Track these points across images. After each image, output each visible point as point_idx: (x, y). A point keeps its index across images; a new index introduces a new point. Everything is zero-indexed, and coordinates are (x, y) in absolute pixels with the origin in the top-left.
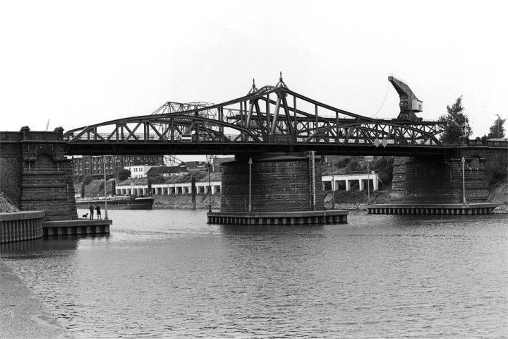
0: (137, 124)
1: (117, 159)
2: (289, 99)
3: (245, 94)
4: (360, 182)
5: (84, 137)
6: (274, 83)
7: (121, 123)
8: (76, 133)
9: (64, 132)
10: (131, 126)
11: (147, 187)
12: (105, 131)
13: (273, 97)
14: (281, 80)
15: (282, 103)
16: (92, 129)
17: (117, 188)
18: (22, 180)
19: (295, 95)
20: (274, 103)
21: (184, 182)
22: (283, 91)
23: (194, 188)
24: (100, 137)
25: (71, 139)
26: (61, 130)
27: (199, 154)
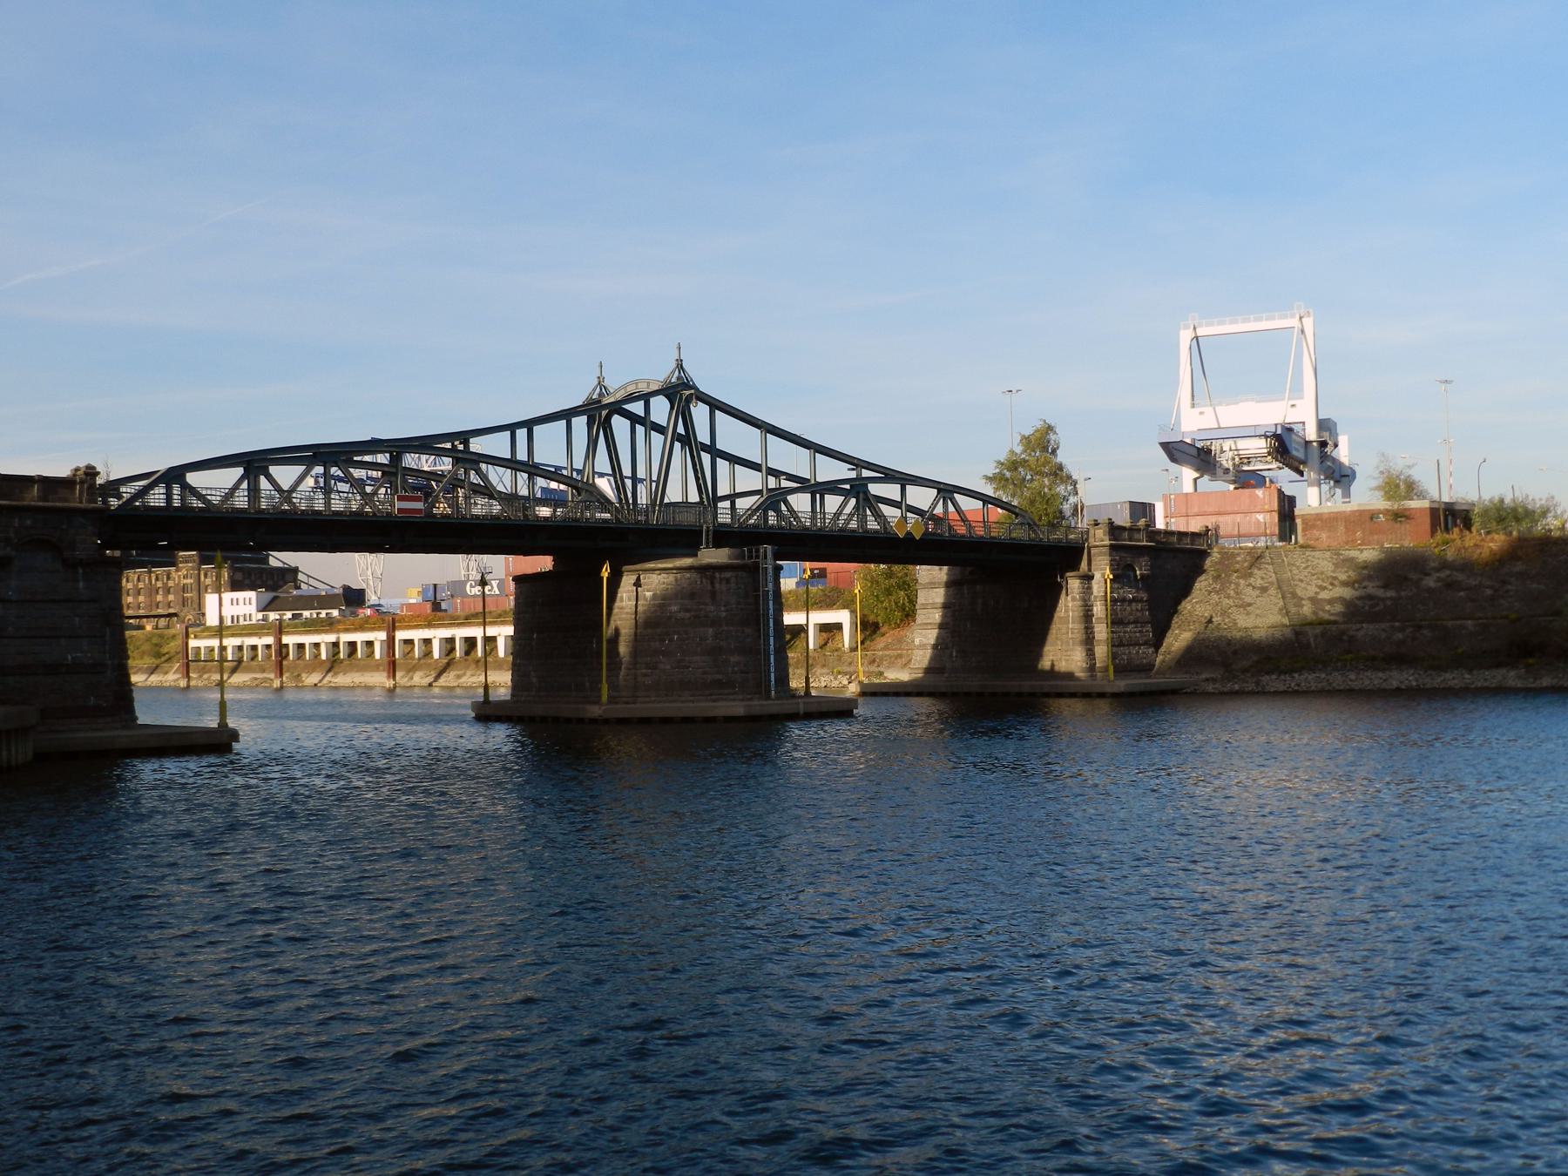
0: (303, 468)
1: (185, 577)
2: (700, 412)
3: (578, 401)
4: (416, 643)
5: (157, 498)
6: (659, 372)
7: (254, 464)
8: (127, 491)
9: (99, 481)
10: (285, 475)
11: (270, 640)
12: (215, 483)
13: (660, 410)
14: (680, 366)
15: (681, 430)
16: (175, 475)
17: (193, 643)
18: (167, 499)
19: (715, 405)
20: (660, 429)
21: (260, 635)
22: (681, 392)
23: (391, 641)
24: (201, 497)
25: (114, 502)
26: (91, 472)
27: (1302, 384)
